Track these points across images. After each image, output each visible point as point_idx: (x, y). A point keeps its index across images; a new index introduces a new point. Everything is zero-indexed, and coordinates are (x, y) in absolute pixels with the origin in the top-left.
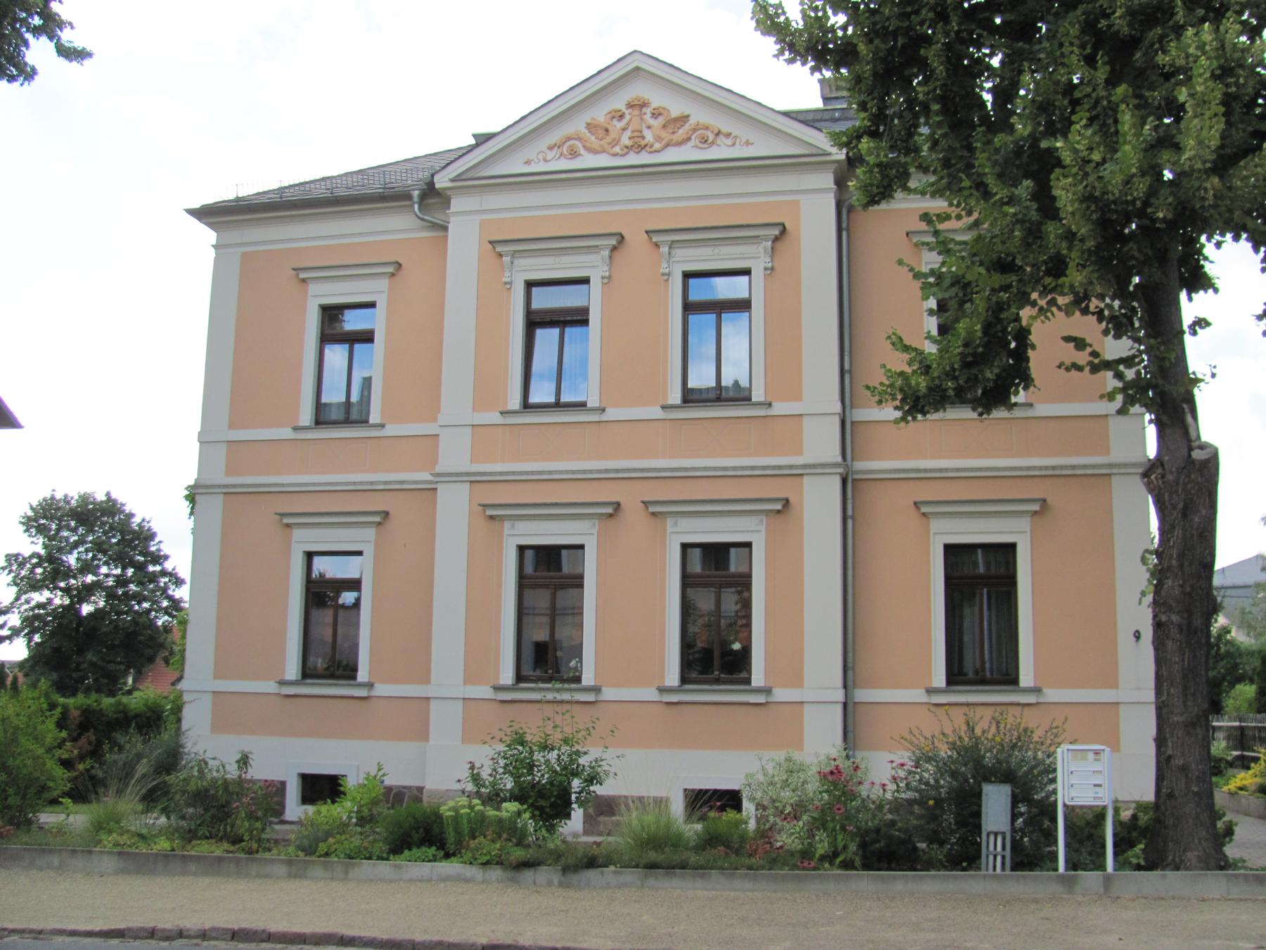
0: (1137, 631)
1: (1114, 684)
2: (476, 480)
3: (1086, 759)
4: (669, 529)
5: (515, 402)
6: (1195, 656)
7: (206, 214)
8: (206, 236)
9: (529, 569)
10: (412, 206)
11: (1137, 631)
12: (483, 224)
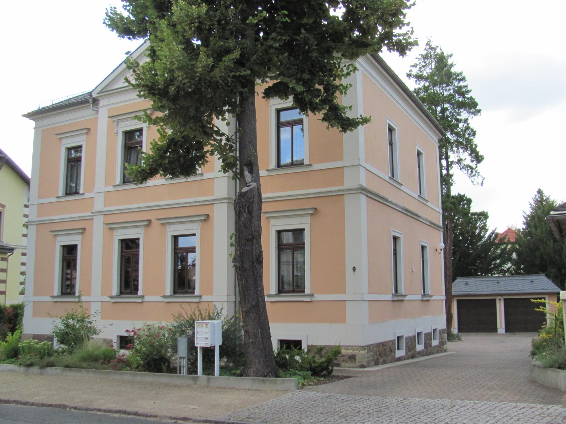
0: (354, 267)
2: (106, 214)
3: (202, 326)
4: (168, 230)
6: (247, 281)
7: (31, 115)
8: (31, 124)
9: (65, 255)
11: (354, 267)
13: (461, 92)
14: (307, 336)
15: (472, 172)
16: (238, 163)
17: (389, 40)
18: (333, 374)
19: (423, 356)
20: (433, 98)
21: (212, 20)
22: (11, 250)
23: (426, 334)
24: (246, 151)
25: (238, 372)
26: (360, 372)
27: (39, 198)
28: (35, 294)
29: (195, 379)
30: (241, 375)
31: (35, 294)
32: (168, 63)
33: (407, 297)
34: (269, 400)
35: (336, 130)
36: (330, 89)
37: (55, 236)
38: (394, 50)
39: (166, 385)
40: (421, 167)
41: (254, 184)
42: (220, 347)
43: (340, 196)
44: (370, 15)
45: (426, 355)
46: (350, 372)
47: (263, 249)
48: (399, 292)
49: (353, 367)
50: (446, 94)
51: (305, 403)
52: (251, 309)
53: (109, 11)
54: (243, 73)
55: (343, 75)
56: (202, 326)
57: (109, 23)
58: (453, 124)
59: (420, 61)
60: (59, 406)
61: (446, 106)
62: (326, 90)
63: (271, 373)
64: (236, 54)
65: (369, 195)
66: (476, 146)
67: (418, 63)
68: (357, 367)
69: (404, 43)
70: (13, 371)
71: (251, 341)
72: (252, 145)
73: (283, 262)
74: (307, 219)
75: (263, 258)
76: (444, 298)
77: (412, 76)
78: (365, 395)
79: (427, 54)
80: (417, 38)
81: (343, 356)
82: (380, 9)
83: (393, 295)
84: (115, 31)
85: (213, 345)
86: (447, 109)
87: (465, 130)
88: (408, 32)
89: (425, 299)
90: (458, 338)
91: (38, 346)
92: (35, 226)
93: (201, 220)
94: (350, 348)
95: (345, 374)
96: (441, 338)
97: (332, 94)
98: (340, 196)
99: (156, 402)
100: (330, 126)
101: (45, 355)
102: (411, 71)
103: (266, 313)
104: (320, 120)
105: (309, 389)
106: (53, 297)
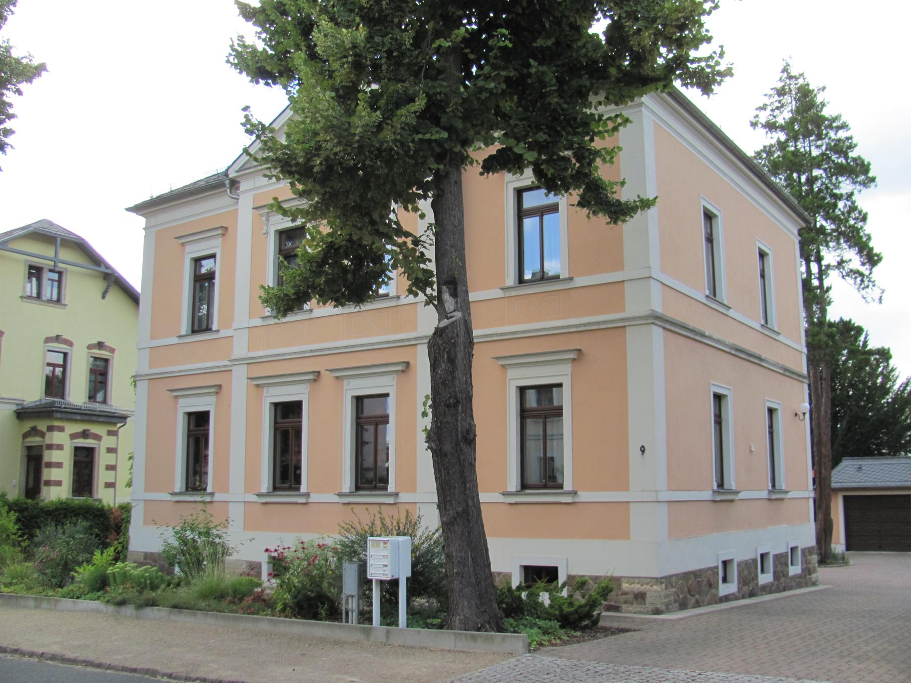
0: (643, 447)
1: (626, 488)
2: (251, 362)
3: (378, 546)
5: (511, 279)
7: (138, 209)
8: (140, 221)
9: (192, 427)
10: (226, 191)
11: (643, 447)
12: (255, 197)
13: (841, 148)
14: (567, 559)
15: (862, 281)
16: (435, 279)
17: (683, 69)
18: (601, 624)
19: (771, 592)
20: (791, 161)
21: (378, 50)
22: (123, 418)
23: (803, 551)
24: (447, 260)
25: (437, 621)
26: (649, 621)
27: (152, 338)
28: (147, 490)
29: (368, 632)
30: (441, 627)
31: (147, 490)
32: (308, 121)
33: (740, 494)
34: (477, 670)
35: (602, 219)
36: (586, 156)
37: (176, 397)
38: (692, 85)
39: (323, 641)
40: (766, 277)
41: (458, 315)
42: (408, 579)
43: (619, 328)
44: (643, 29)
45: (778, 590)
46: (633, 620)
47: (476, 422)
48: (726, 486)
49: (641, 612)
50: (815, 153)
51: (531, 677)
52: (455, 520)
53: (236, 42)
54: (436, 137)
55: (607, 131)
56: (378, 546)
57: (236, 61)
58: (828, 203)
59: (772, 100)
60: (147, 671)
61: (816, 172)
62: (579, 157)
63: (489, 623)
64: (420, 104)
65: (668, 326)
66: (869, 237)
67: (769, 104)
68: (647, 613)
69: (709, 73)
70: (98, 611)
71: (455, 571)
72: (456, 251)
73: (530, 436)
74: (567, 368)
75: (475, 435)
76: (812, 494)
77: (760, 126)
78: (637, 664)
79: (783, 88)
80: (732, 64)
81: (625, 593)
82: (660, 17)
83: (714, 492)
84: (244, 73)
85: (396, 577)
86: (816, 179)
87: (849, 212)
88: (713, 55)
89: (774, 497)
90: (841, 561)
91: (136, 573)
92: (146, 382)
93: (398, 371)
94: (637, 580)
95: (623, 625)
96: (806, 560)
97: (590, 164)
98: (619, 328)
99: (296, 668)
100: (591, 215)
101: (146, 586)
102: (757, 116)
103: (482, 526)
104: (573, 205)
105: (547, 652)
106: (173, 494)
